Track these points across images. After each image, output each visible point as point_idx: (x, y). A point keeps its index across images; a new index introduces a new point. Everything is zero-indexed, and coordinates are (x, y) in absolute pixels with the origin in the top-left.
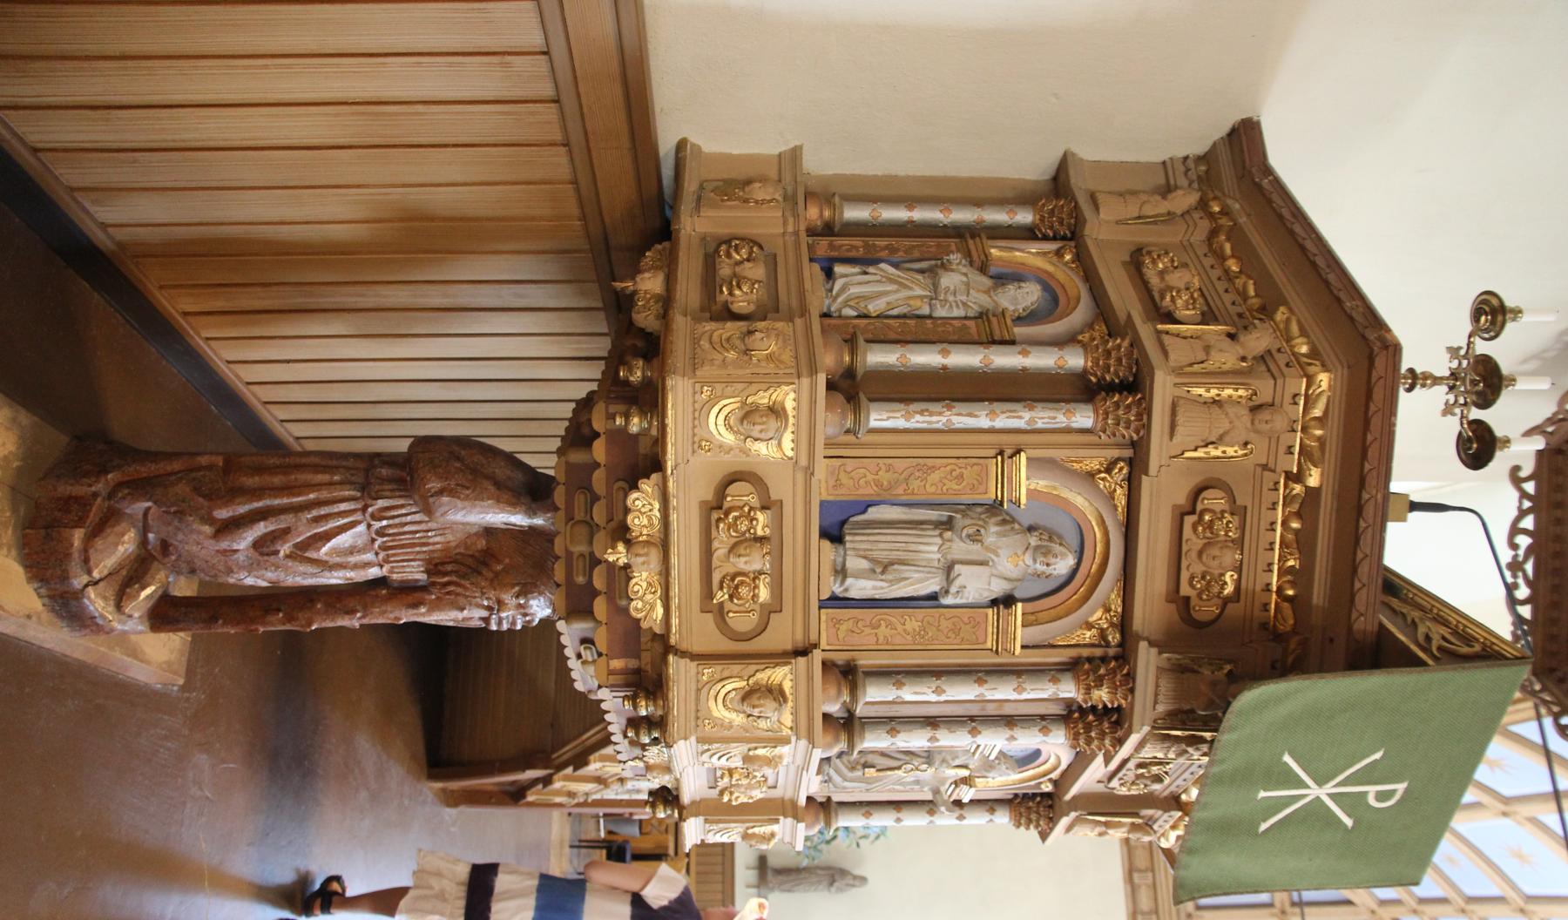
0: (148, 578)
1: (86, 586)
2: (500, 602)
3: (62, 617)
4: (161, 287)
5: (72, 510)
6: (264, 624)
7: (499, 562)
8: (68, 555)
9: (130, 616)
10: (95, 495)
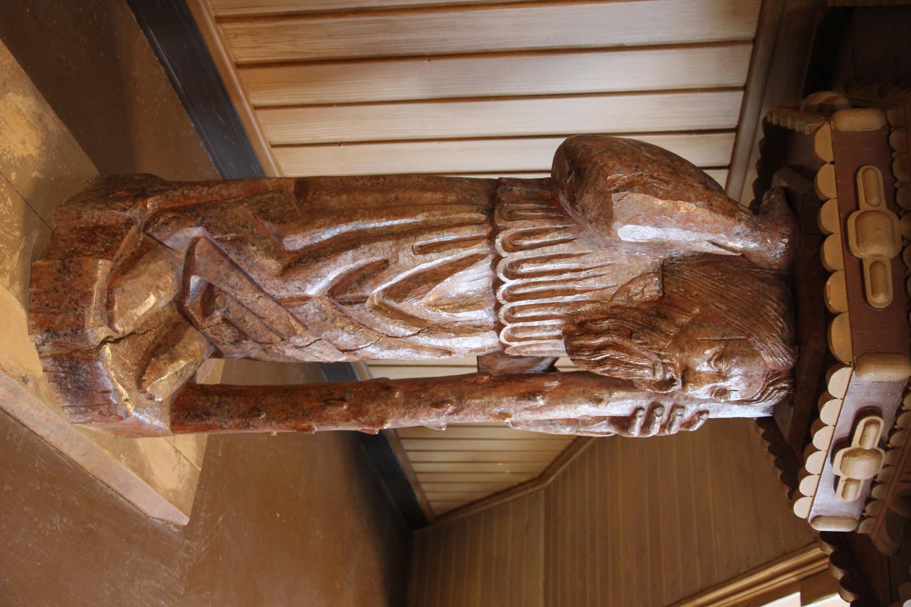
0: (179, 348)
1: (104, 342)
2: (687, 375)
3: (65, 390)
4: (219, 20)
5: (100, 238)
6: (320, 420)
7: (685, 312)
8: (87, 296)
9: (151, 398)
10: (129, 223)
